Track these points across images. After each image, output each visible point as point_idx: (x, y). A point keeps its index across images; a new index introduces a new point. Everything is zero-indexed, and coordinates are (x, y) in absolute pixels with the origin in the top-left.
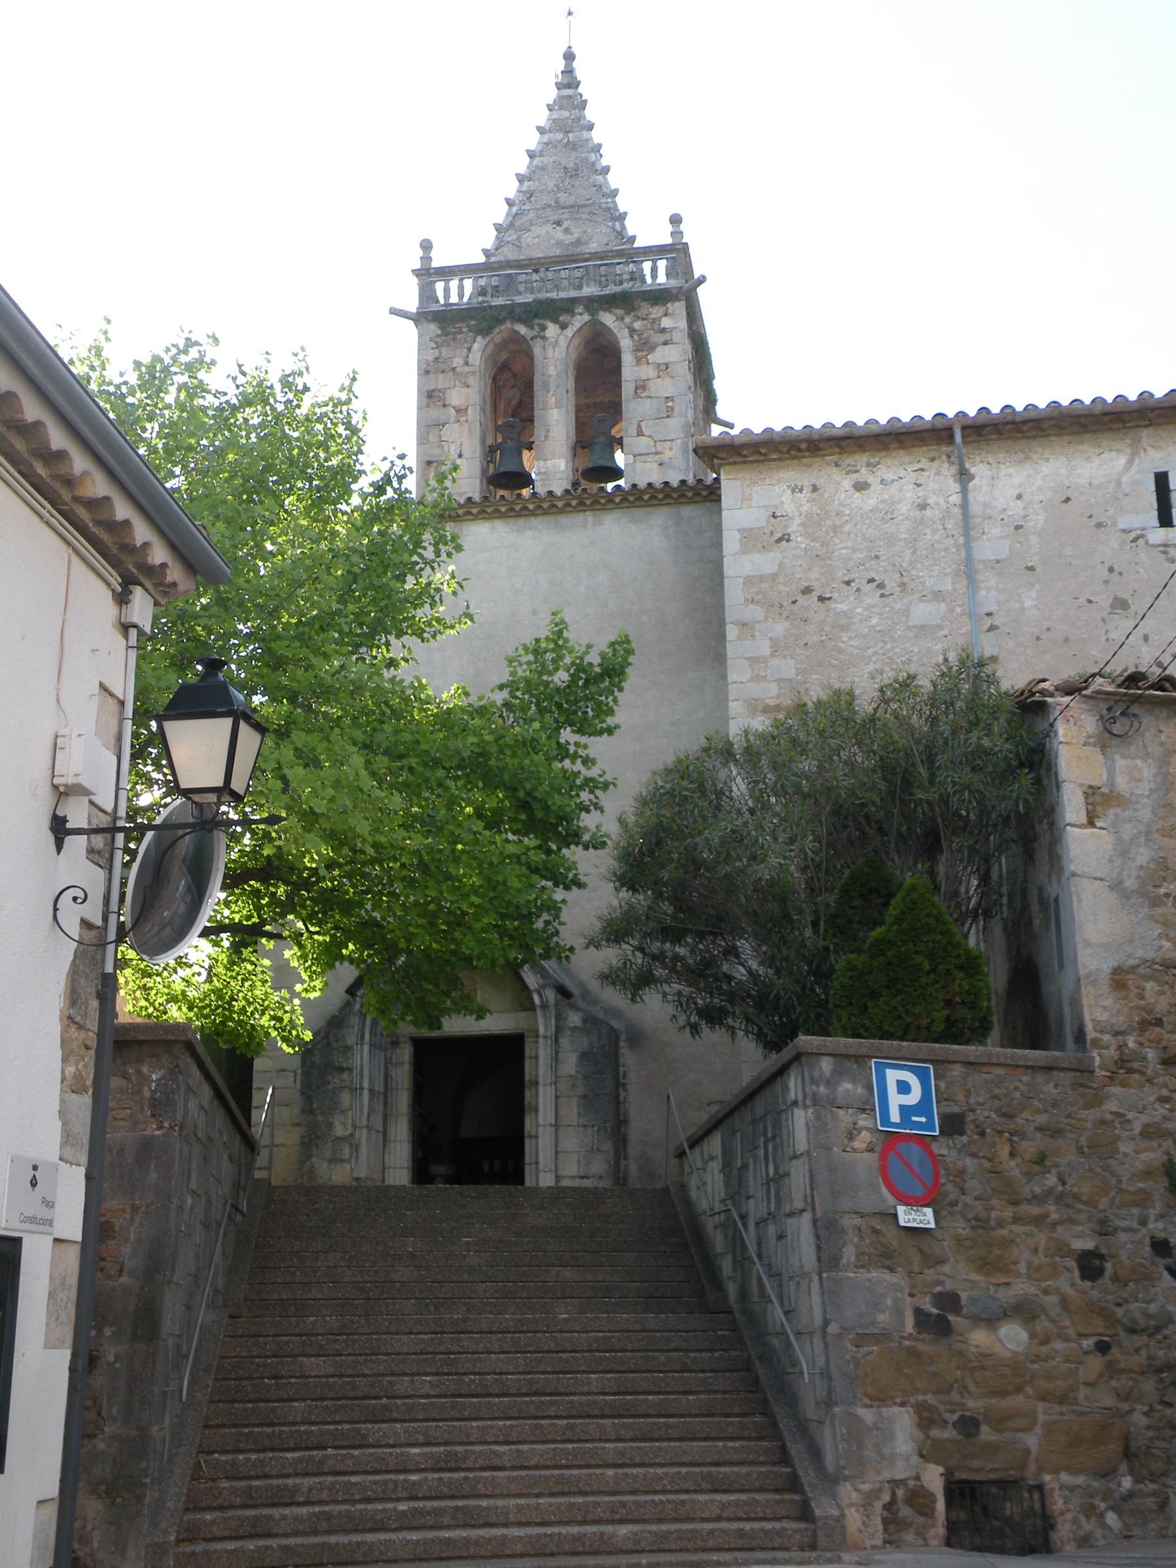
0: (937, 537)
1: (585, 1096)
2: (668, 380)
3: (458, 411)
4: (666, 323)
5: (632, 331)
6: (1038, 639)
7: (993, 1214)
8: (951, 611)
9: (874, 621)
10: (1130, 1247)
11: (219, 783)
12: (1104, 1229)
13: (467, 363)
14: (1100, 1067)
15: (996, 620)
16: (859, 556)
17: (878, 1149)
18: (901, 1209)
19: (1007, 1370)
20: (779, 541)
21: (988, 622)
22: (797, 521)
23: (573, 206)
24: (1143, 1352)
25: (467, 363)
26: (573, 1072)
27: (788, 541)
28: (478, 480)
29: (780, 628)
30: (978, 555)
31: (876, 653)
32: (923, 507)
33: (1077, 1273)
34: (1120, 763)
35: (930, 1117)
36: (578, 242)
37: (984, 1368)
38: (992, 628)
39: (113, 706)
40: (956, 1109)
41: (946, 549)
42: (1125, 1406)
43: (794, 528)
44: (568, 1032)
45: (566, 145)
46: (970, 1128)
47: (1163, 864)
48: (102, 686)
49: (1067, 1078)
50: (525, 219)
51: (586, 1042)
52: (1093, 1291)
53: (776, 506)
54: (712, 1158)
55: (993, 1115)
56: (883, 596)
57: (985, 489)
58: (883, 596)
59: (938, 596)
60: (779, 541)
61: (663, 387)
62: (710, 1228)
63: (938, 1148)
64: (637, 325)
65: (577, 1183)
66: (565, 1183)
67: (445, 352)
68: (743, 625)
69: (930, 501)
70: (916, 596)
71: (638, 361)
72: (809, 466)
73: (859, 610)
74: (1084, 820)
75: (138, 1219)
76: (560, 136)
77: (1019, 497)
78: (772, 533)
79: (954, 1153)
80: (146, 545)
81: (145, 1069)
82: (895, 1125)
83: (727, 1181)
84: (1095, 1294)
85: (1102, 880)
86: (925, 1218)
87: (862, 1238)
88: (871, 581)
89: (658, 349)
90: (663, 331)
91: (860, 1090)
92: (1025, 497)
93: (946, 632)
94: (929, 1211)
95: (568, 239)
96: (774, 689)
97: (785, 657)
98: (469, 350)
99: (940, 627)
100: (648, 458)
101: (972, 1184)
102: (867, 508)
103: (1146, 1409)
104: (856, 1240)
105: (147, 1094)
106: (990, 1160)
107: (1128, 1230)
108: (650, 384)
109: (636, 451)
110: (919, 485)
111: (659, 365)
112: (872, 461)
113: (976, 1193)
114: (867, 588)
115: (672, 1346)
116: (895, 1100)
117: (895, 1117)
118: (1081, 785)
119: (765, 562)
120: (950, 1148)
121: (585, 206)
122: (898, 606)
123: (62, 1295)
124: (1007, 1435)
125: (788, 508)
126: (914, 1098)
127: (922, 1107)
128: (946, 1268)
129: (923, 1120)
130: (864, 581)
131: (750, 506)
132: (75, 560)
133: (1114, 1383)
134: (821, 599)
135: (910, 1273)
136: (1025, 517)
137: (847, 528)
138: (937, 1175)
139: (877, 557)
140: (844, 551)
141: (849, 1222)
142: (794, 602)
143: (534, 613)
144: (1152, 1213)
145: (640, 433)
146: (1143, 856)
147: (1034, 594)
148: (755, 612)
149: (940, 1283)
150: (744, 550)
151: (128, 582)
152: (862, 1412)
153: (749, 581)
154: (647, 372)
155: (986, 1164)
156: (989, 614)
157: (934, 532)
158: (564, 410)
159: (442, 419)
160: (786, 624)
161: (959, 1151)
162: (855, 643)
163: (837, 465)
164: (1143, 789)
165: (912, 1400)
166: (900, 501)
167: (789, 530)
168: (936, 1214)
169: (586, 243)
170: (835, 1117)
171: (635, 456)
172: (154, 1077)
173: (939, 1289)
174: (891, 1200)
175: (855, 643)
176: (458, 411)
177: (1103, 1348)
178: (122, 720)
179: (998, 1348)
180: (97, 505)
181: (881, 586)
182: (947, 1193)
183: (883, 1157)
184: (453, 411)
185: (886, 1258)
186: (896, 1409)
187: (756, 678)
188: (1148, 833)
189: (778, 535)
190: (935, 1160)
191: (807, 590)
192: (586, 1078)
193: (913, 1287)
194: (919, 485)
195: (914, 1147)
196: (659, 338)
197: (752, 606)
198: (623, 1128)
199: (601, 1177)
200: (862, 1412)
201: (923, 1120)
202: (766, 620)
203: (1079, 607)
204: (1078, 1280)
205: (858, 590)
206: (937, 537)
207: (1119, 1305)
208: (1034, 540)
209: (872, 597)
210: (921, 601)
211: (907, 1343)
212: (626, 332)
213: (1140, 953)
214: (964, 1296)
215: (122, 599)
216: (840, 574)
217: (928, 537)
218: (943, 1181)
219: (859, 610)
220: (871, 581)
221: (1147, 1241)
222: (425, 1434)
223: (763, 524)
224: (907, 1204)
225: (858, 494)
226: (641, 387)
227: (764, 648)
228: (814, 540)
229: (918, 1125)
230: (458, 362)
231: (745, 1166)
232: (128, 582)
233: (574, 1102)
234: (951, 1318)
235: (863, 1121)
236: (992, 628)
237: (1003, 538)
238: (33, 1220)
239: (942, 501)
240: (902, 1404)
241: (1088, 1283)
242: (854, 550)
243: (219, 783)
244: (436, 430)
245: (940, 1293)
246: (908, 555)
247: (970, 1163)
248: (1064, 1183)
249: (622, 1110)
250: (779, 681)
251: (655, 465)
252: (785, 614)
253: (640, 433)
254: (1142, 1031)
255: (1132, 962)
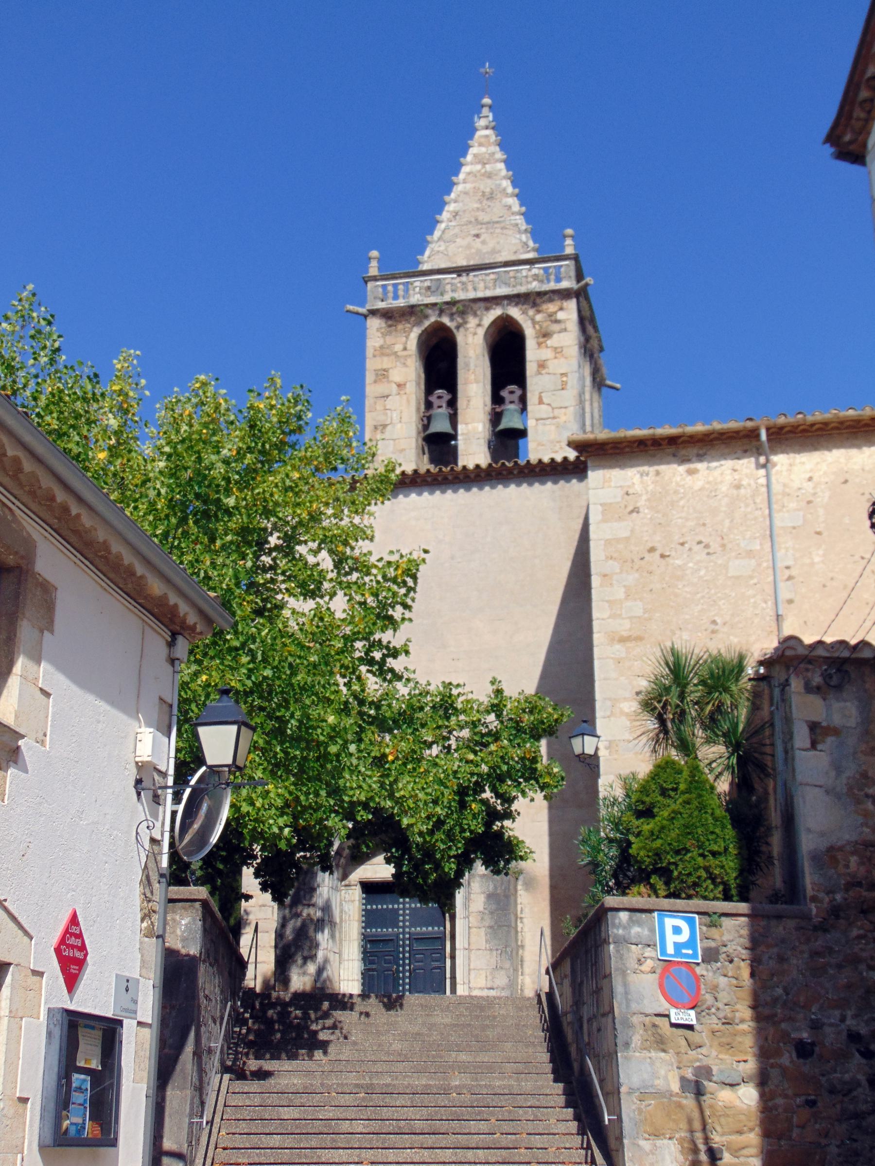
0: (749, 510)
1: (491, 927)
2: (562, 360)
3: (399, 385)
4: (560, 315)
5: (534, 322)
6: (824, 586)
7: (737, 1014)
8: (759, 565)
9: (702, 573)
10: (831, 1037)
11: (229, 761)
12: (816, 1026)
13: (405, 349)
14: (817, 916)
15: (794, 572)
16: (691, 524)
17: (659, 971)
18: (673, 1012)
19: (742, 1117)
20: (632, 512)
21: (787, 573)
22: (644, 497)
23: (488, 223)
24: (838, 1106)
25: (405, 349)
26: (481, 909)
27: (638, 512)
28: (414, 440)
29: (631, 578)
30: (777, 523)
31: (703, 597)
32: (738, 487)
33: (794, 1055)
34: (836, 705)
35: (695, 949)
36: (494, 252)
37: (728, 1116)
38: (790, 578)
39: (166, 708)
40: (713, 944)
41: (755, 519)
42: (823, 1141)
43: (642, 503)
44: (478, 879)
45: (483, 175)
46: (722, 957)
47: (864, 775)
48: (161, 699)
49: (791, 924)
50: (452, 233)
51: (491, 887)
52: (807, 1067)
53: (629, 487)
54: (566, 976)
55: (739, 948)
56: (708, 554)
57: (785, 473)
58: (708, 554)
59: (750, 554)
60: (632, 512)
61: (557, 366)
62: (565, 1024)
63: (699, 970)
64: (539, 317)
65: (485, 993)
66: (475, 993)
67: (389, 340)
68: (605, 576)
69: (744, 483)
70: (733, 554)
71: (539, 344)
72: (654, 456)
73: (691, 565)
74: (808, 745)
75: (174, 1014)
76: (479, 167)
77: (810, 479)
78: (626, 507)
79: (711, 974)
80: (186, 614)
81: (178, 917)
82: (671, 955)
83: (574, 993)
84: (806, 1069)
85: (821, 787)
86: (690, 1017)
87: (646, 1030)
88: (699, 543)
89: (555, 336)
90: (557, 321)
91: (646, 932)
92: (815, 479)
93: (755, 581)
94: (692, 1013)
95: (485, 249)
96: (627, 624)
97: (635, 600)
98: (407, 337)
99: (751, 577)
100: (548, 422)
101: (724, 997)
102: (696, 488)
103: (838, 1143)
104: (641, 1032)
105: (179, 932)
106: (737, 979)
107: (831, 1025)
108: (549, 363)
109: (538, 416)
110: (735, 470)
111: (556, 348)
112: (701, 452)
113: (725, 1001)
114: (696, 548)
115: (529, 1104)
116: (671, 939)
117: (670, 950)
118: (807, 722)
119: (621, 529)
120: (707, 970)
121: (497, 222)
122: (720, 562)
123: (142, 1053)
124: (742, 1159)
125: (638, 488)
126: (684, 937)
127: (691, 943)
128: (704, 1050)
129: (690, 952)
130: (694, 543)
131: (610, 487)
132: (146, 627)
133: (817, 1126)
134: (663, 556)
135: (678, 1053)
136: (815, 494)
137: (682, 503)
138: (698, 989)
139: (704, 525)
140: (680, 521)
141: (635, 1020)
142: (642, 559)
143: (452, 558)
144: (849, 1013)
145: (541, 402)
146: (851, 770)
147: (821, 552)
148: (613, 566)
149: (698, 1060)
150: (604, 521)
151: (174, 635)
152: (642, 1143)
153: (608, 542)
154: (546, 354)
155: (734, 982)
156: (788, 568)
157: (747, 506)
158: (481, 384)
159: (386, 393)
160: (637, 575)
161: (715, 972)
162: (687, 589)
163: (674, 455)
164: (852, 722)
165: (677, 1136)
166: (722, 482)
167: (638, 505)
168: (698, 1014)
169: (500, 252)
170: (629, 950)
171: (537, 420)
172: (183, 922)
173: (698, 1064)
174: (666, 1005)
175: (687, 589)
176: (399, 385)
177: (811, 1104)
178: (171, 715)
179: (738, 1103)
180: (162, 601)
181: (707, 546)
182: (706, 1000)
183: (661, 977)
184: (394, 386)
185: (661, 1044)
186: (666, 1141)
187: (613, 616)
188: (855, 753)
189: (630, 508)
190: (697, 978)
191: (652, 550)
192: (492, 913)
193: (680, 1062)
194: (735, 470)
195: (683, 969)
196: (555, 327)
197: (611, 562)
198: (520, 952)
199: (503, 989)
200: (642, 1143)
201: (690, 952)
202: (621, 572)
203: (855, 562)
204: (795, 1059)
205: (690, 549)
206: (749, 510)
207: (823, 1075)
208: (821, 511)
209: (700, 554)
210: (737, 558)
211: (674, 1099)
212: (529, 323)
213: (847, 837)
214: (715, 1069)
215: (171, 644)
216: (677, 538)
217: (743, 509)
218: (703, 992)
219: (691, 565)
220: (699, 543)
221: (845, 1033)
222: (358, 1156)
223: (619, 500)
224: (677, 1008)
225: (690, 477)
226: (542, 365)
227: (620, 594)
228: (658, 512)
229: (687, 956)
230: (398, 347)
231: (582, 982)
232: (174, 635)
233: (482, 931)
234: (705, 1083)
235: (649, 952)
236: (790, 578)
237: (798, 510)
238: (126, 1010)
239: (752, 482)
240: (670, 1138)
241: (801, 1061)
242: (687, 519)
243: (229, 761)
244: (382, 401)
245: (699, 1067)
246: (727, 523)
247: (723, 981)
248: (787, 994)
249: (520, 938)
250: (630, 618)
251: (553, 428)
252: (636, 567)
253: (541, 402)
254: (847, 890)
255: (839, 844)
